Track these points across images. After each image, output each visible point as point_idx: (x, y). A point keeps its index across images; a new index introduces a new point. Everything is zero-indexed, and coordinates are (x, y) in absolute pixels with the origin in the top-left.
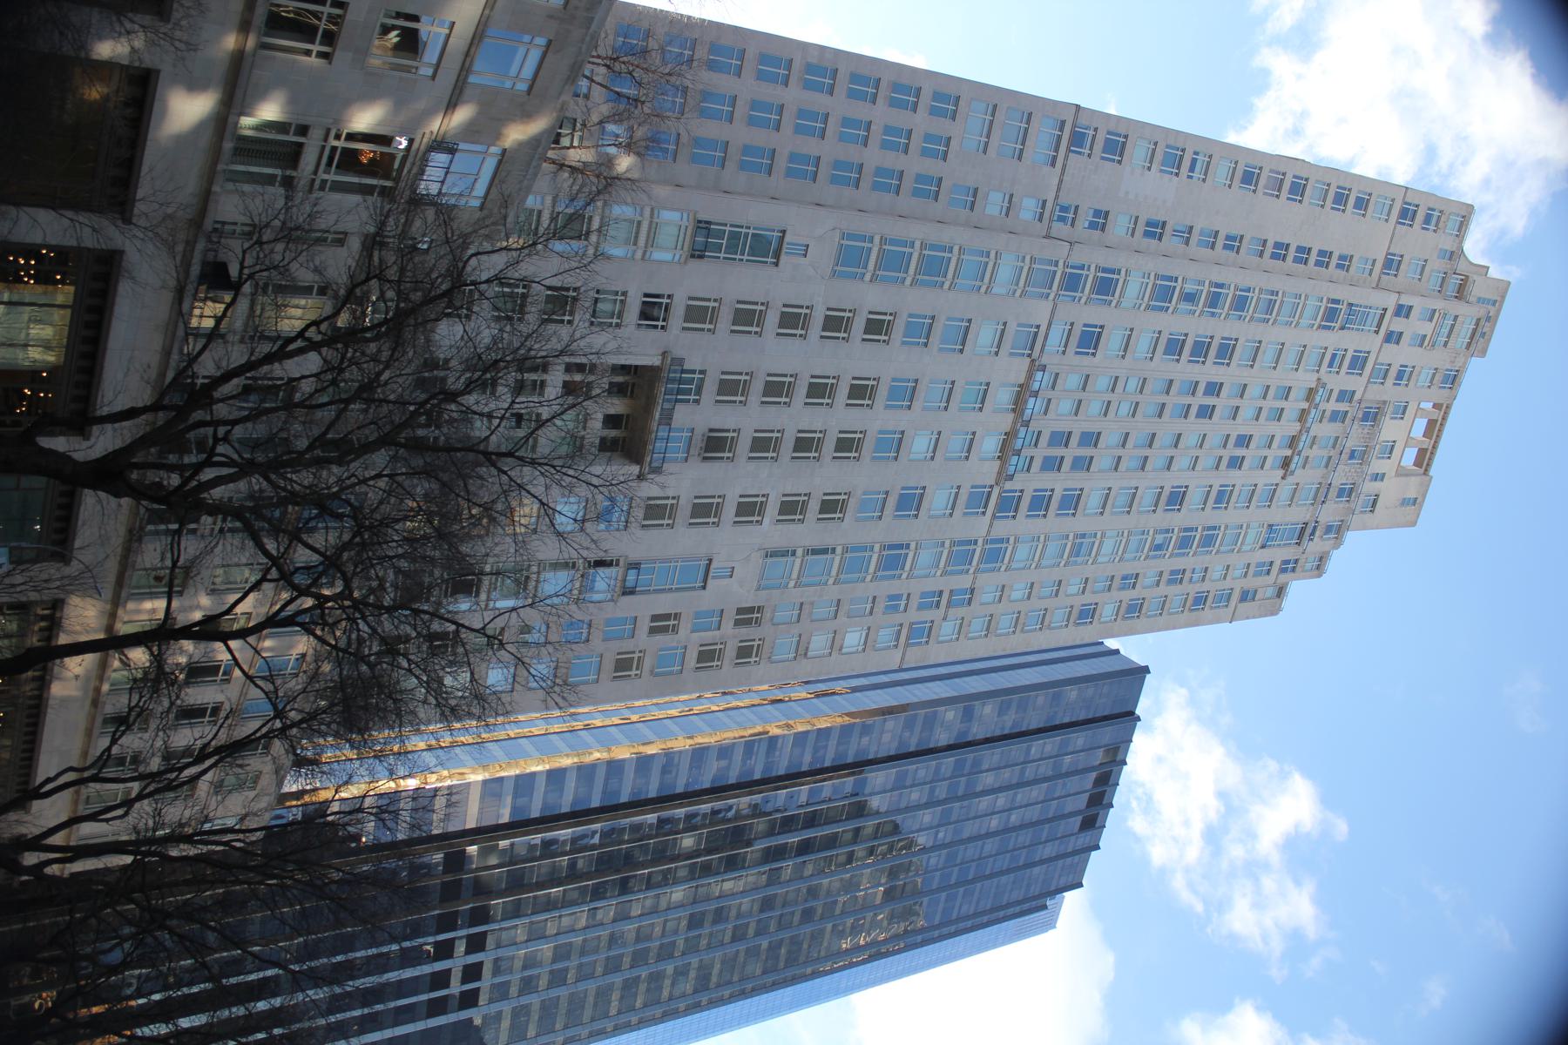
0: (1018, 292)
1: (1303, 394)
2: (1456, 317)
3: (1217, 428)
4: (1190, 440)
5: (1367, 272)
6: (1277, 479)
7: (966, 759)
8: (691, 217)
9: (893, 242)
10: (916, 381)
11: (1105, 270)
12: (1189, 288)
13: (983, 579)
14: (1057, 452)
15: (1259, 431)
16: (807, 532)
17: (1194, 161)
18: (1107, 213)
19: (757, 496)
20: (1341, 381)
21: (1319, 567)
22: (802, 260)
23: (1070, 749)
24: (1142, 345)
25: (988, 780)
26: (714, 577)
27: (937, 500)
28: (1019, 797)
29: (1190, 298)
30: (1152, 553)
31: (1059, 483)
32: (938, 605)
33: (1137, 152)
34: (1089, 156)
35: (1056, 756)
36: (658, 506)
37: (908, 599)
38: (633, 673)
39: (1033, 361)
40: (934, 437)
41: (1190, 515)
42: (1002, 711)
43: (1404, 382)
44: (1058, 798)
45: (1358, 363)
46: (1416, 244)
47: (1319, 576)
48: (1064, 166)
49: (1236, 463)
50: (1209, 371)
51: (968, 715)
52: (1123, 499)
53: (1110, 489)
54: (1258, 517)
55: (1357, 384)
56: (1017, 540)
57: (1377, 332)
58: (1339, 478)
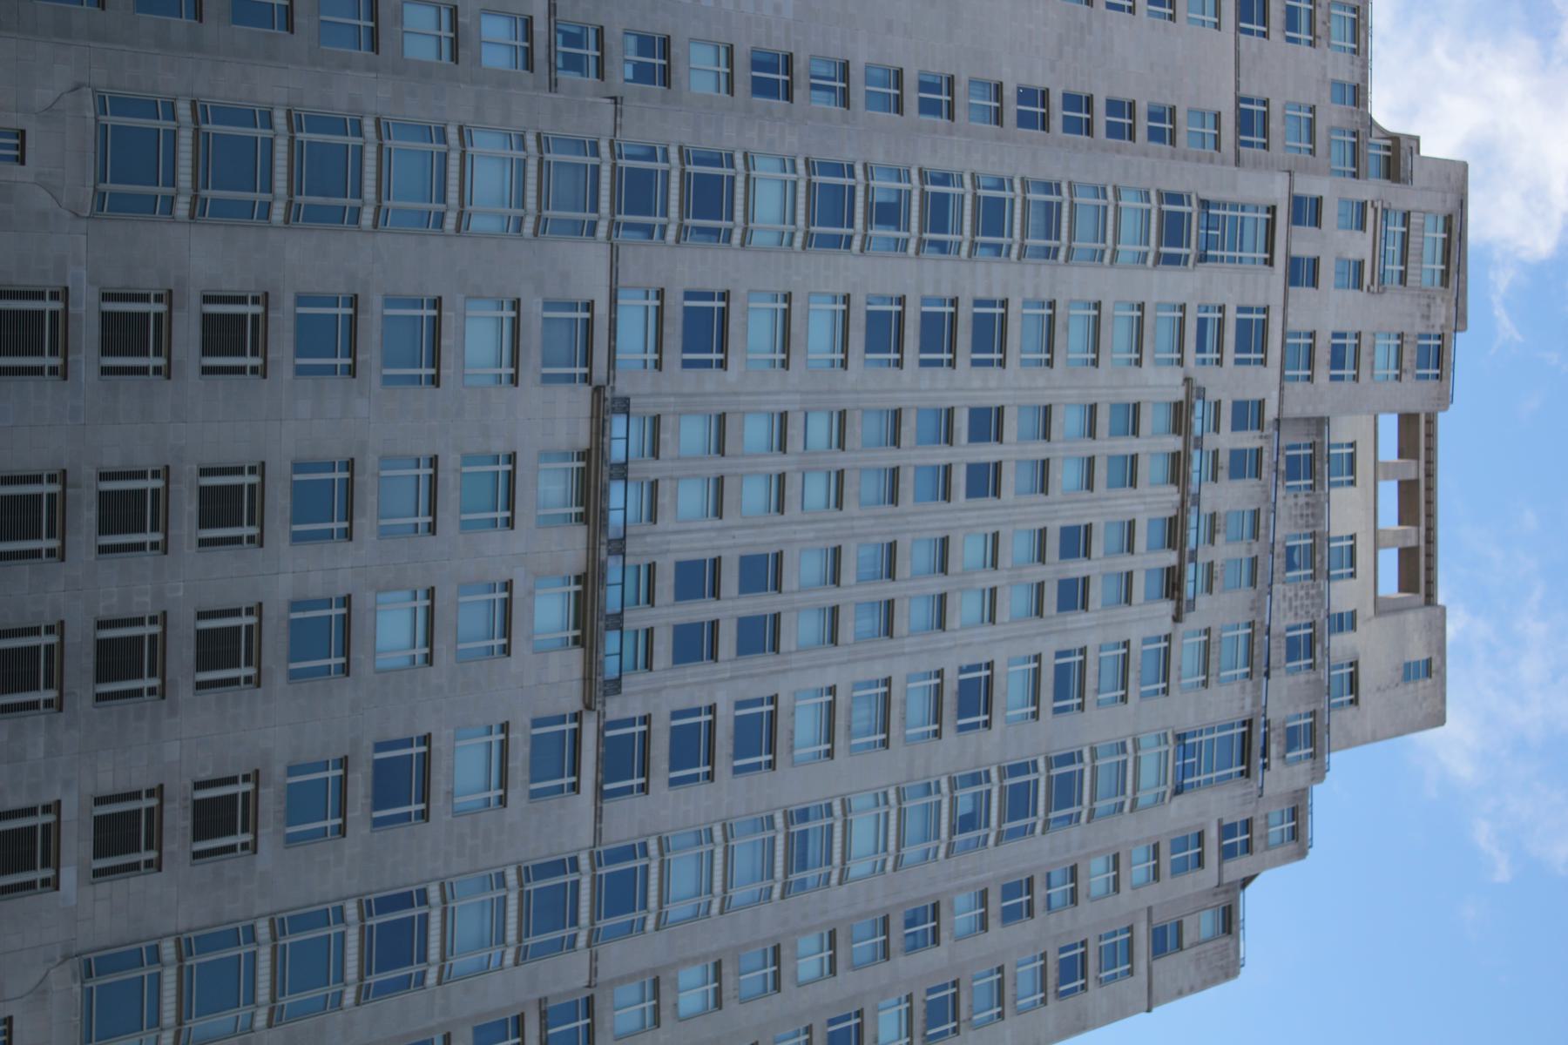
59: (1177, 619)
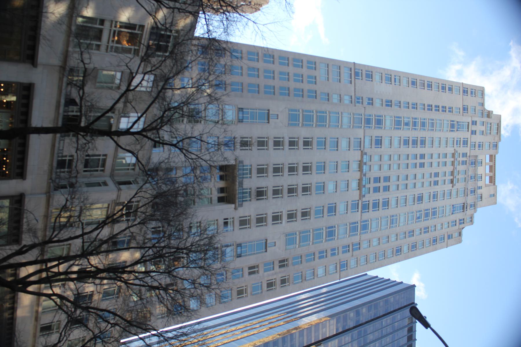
0: (351, 127)
1: (451, 155)
2: (491, 124)
3: (427, 170)
4: (419, 176)
5: (458, 112)
6: (451, 188)
7: (361, 331)
8: (236, 107)
9: (307, 111)
10: (325, 163)
11: (329, 228)
12: (406, 120)
13: (363, 237)
14: (377, 185)
15: (441, 170)
16: (298, 225)
17: (395, 79)
18: (372, 99)
19: (278, 212)
20: (462, 150)
21: (472, 221)
22: (277, 120)
23: (396, 320)
24: (396, 143)
25: (371, 337)
26: (269, 247)
27: (341, 208)
28: (383, 342)
29: (407, 124)
30: (417, 220)
31: (381, 196)
32: (349, 251)
33: (377, 77)
34: (362, 79)
35: (392, 324)
36: (244, 220)
37: (338, 250)
38: (244, 295)
39: (362, 151)
40: (335, 183)
41: (425, 205)
42: (369, 310)
43: (481, 148)
44: (397, 340)
45: (465, 143)
46: (471, 101)
47: (472, 224)
48: (355, 83)
49: (436, 183)
50: (419, 150)
51: (358, 313)
52: (403, 201)
53: (397, 197)
54: (447, 203)
55: (467, 150)
56: (371, 220)
57: (468, 131)
58: (470, 187)
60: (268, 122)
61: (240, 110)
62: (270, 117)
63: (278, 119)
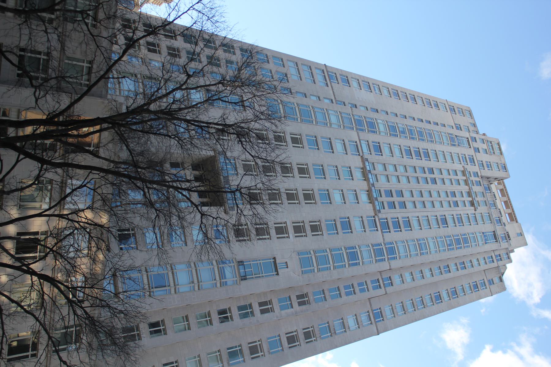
20: (471, 168)
39: (361, 157)
41: (452, 230)
48: (332, 86)
50: (424, 163)
59: (475, 210)
60: (278, 274)
61: (240, 264)
62: (278, 267)
63: (287, 267)
